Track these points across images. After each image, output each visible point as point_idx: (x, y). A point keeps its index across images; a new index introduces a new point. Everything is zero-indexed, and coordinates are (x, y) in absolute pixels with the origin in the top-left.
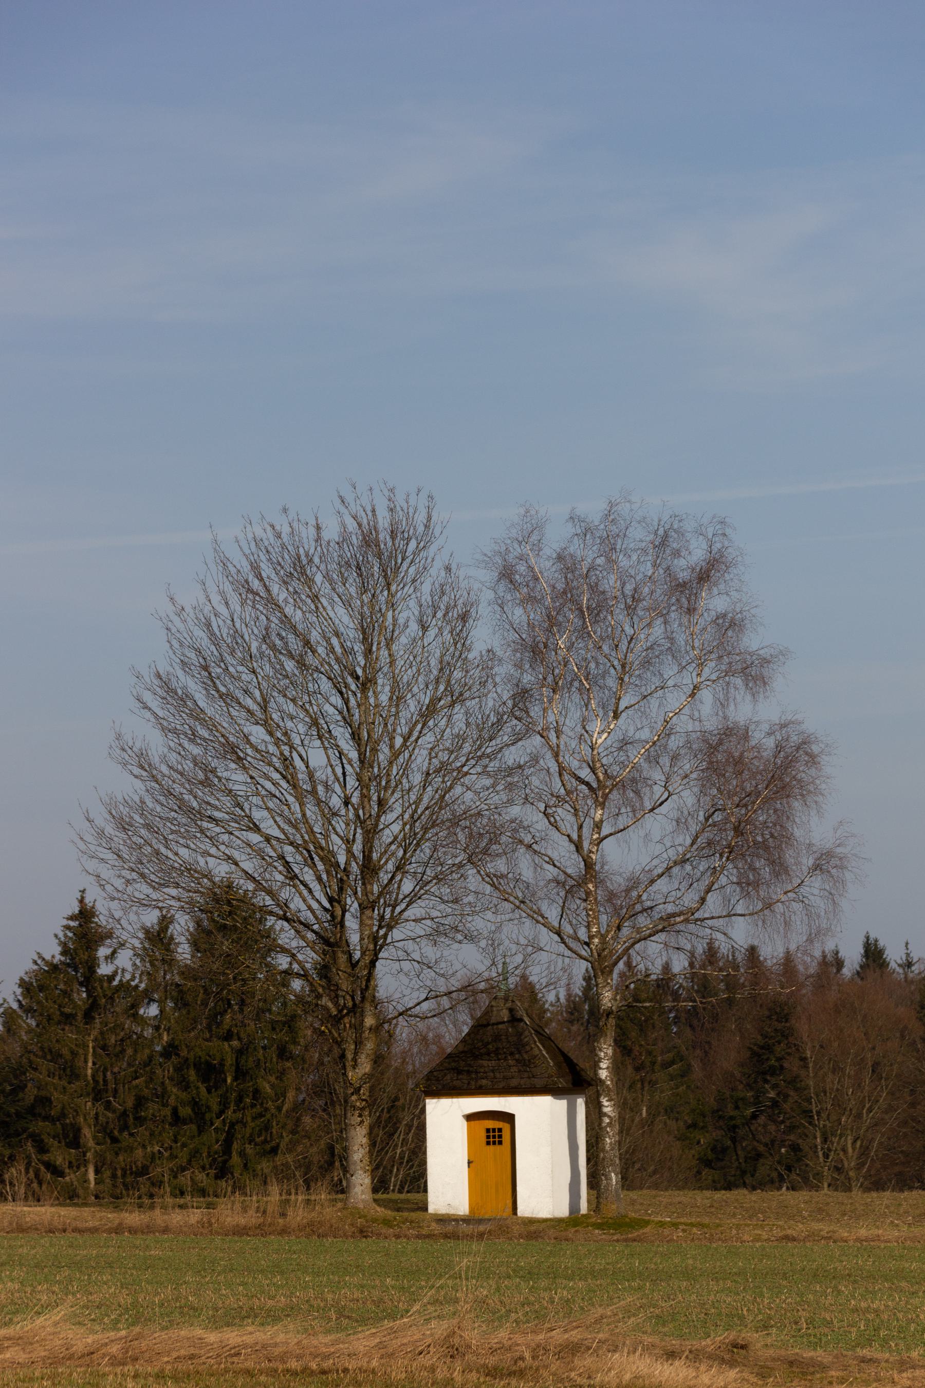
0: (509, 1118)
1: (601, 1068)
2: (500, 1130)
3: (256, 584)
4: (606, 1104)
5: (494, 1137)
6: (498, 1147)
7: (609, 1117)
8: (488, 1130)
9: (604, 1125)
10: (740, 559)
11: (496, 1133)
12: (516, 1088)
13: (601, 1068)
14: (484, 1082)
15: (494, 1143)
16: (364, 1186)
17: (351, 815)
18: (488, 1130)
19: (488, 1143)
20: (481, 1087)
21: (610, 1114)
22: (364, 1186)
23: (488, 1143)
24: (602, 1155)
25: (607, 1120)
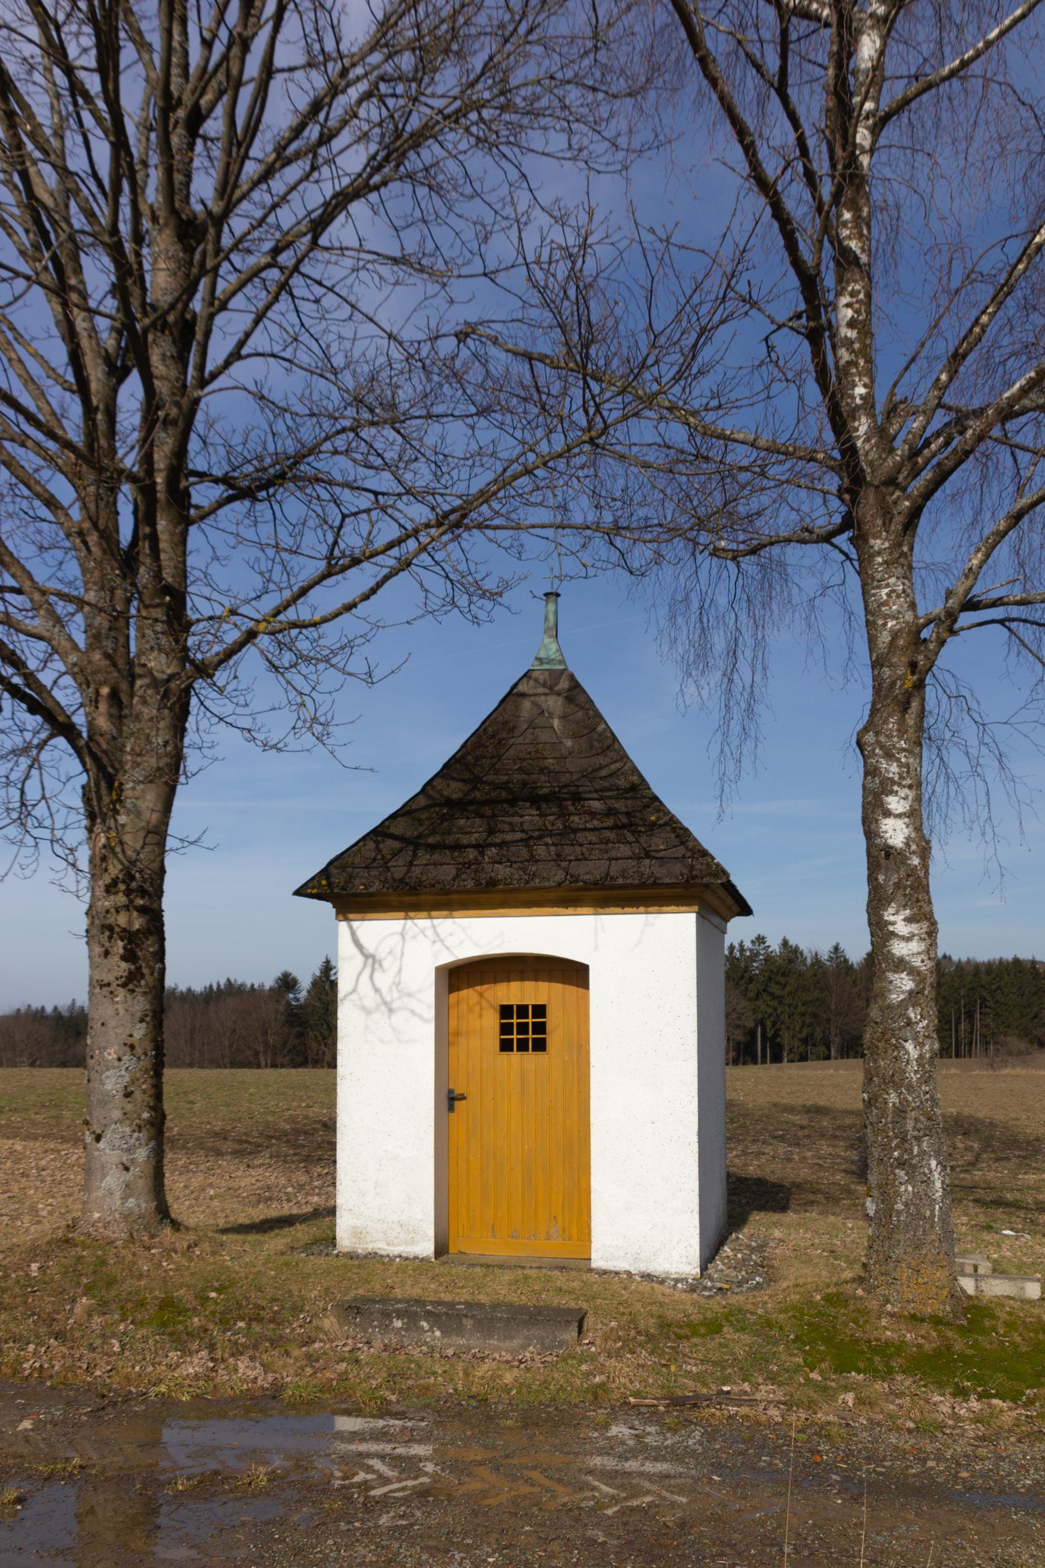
0: (574, 973)
1: (888, 814)
2: (540, 1010)
3: (80, 101)
4: (901, 928)
5: (523, 1028)
6: (530, 1058)
7: (913, 972)
8: (506, 1011)
9: (895, 998)
10: (265, 531)
11: (520, 1014)
12: (596, 885)
13: (888, 814)
14: (502, 871)
15: (523, 1046)
16: (135, 1170)
17: (543, 15)
18: (506, 1011)
19: (506, 1046)
20: (492, 883)
21: (917, 962)
22: (135, 1170)
23: (506, 1046)
24: (893, 1098)
25: (905, 983)
